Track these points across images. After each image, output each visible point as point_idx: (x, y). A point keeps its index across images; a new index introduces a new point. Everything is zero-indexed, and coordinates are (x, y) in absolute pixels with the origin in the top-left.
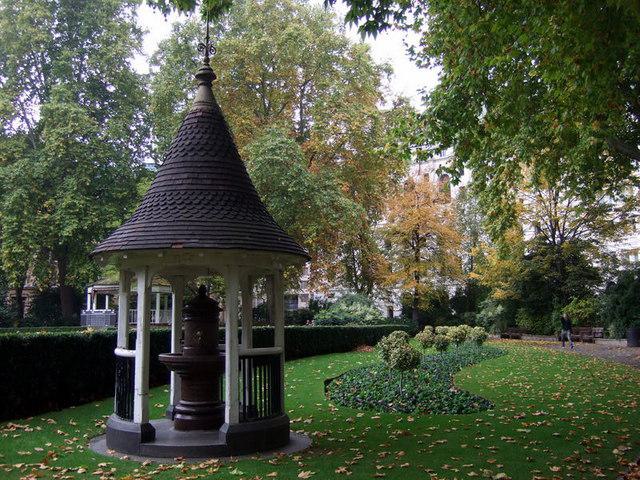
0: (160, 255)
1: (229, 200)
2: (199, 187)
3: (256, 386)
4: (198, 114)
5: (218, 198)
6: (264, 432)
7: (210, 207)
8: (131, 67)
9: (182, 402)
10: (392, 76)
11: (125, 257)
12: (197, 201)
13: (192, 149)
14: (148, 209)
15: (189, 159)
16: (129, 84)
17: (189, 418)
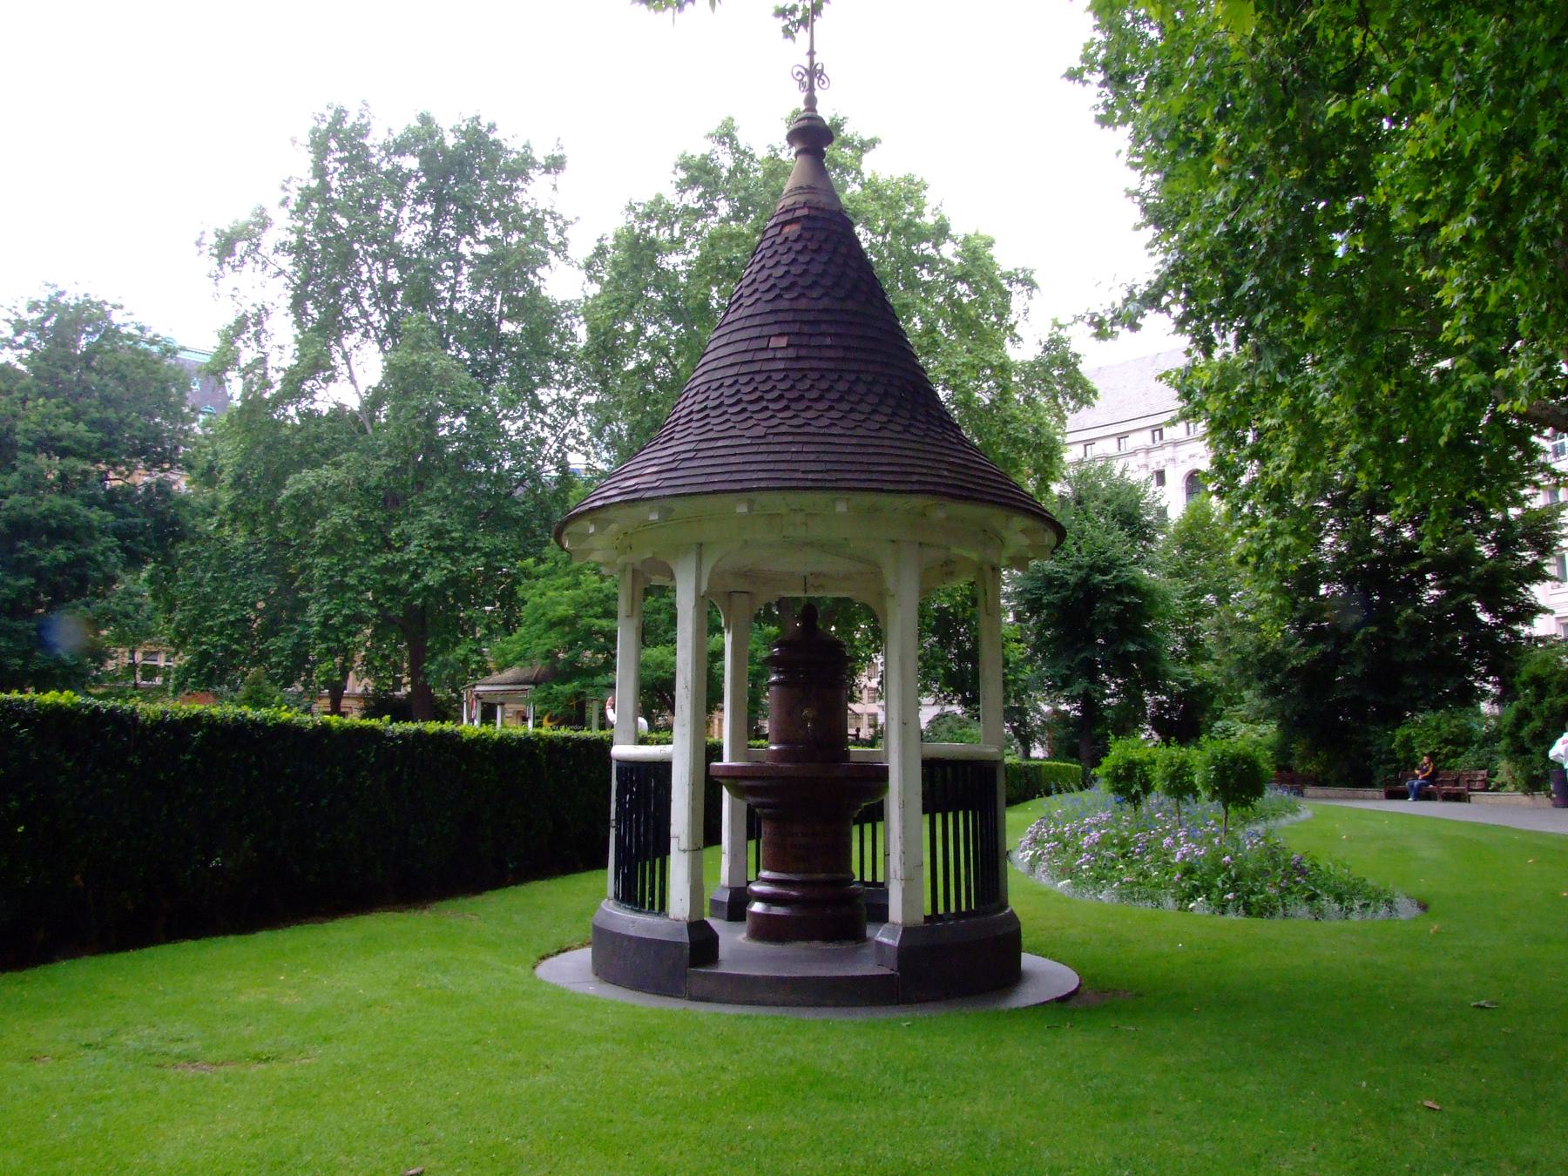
0: (742, 509)
1: (886, 394)
2: (815, 364)
3: (652, 894)
4: (799, 213)
5: (861, 388)
6: (969, 958)
7: (845, 406)
8: (544, 293)
9: (765, 874)
10: (1035, 291)
11: (654, 517)
12: (814, 394)
13: (793, 285)
14: (696, 417)
15: (784, 304)
16: (541, 317)
17: (777, 911)
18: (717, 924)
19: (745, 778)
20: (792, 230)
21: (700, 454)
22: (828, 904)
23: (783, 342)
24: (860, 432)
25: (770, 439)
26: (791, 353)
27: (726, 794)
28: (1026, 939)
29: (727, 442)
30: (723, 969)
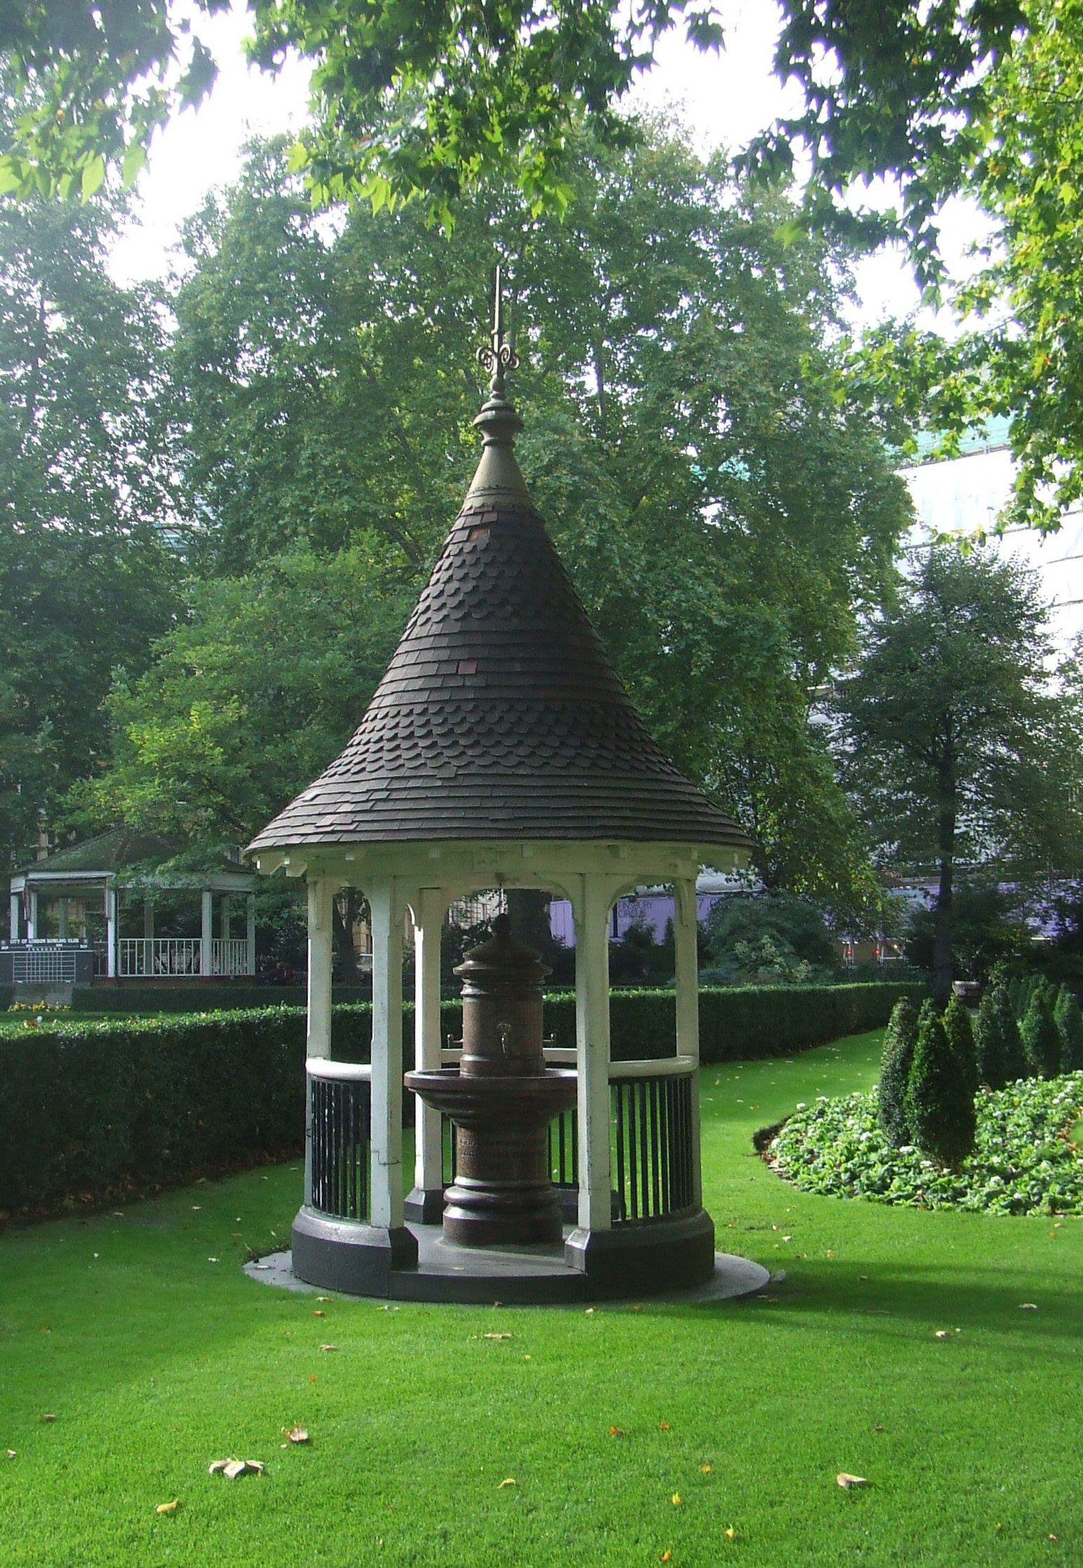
18: (416, 1230)
19: (442, 1091)
20: (482, 537)
21: (394, 795)
22: (519, 1209)
23: (471, 669)
24: (547, 771)
25: (460, 781)
26: (479, 681)
27: (419, 1101)
28: (719, 1234)
29: (418, 783)
30: (421, 1272)
